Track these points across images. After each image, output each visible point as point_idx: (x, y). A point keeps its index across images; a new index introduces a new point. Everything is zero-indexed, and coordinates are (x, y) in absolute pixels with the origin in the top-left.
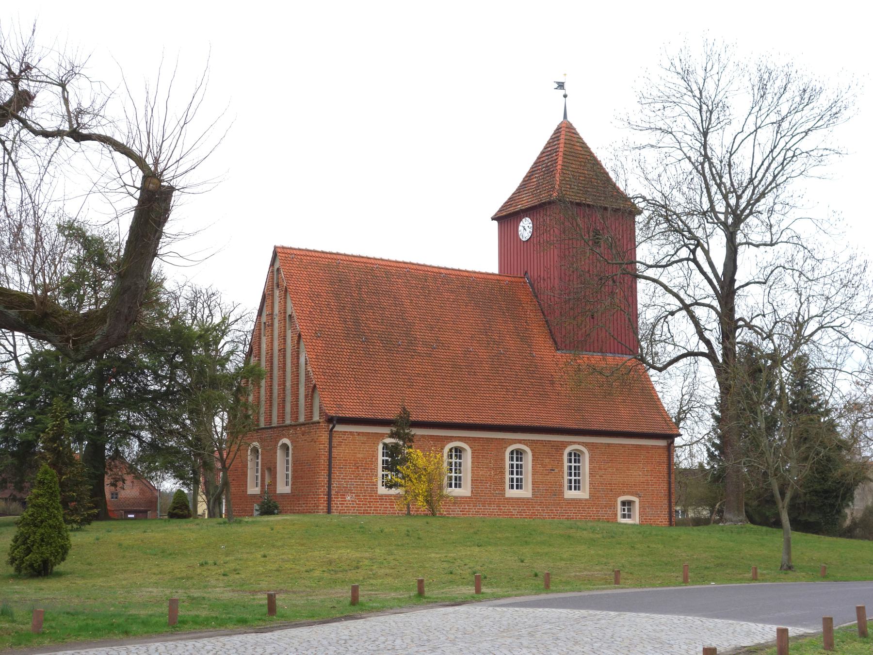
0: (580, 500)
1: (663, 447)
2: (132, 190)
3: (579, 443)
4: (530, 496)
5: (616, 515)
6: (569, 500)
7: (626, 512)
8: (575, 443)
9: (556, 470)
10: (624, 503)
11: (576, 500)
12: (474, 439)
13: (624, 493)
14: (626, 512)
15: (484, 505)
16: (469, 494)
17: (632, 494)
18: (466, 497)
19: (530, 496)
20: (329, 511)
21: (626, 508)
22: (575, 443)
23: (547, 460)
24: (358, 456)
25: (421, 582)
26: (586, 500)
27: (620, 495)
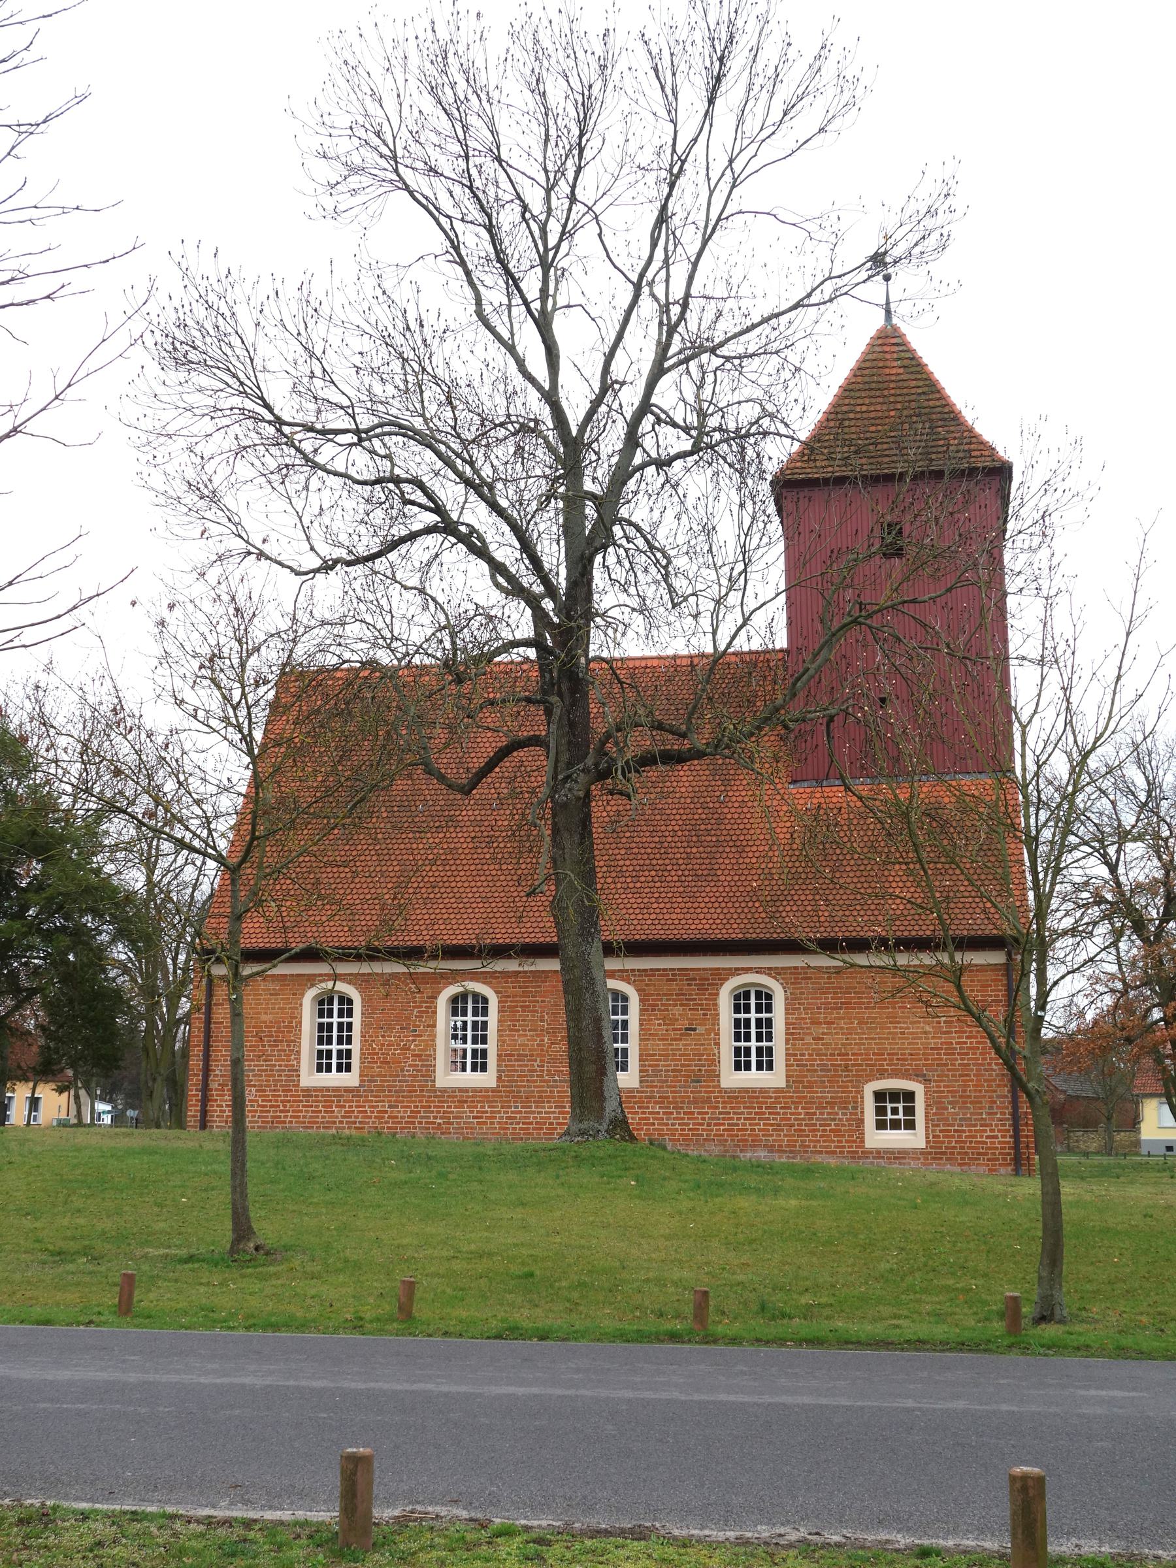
0: (763, 1091)
1: (994, 967)
2: (447, 544)
3: (758, 971)
4: (783, 1085)
5: (861, 1121)
6: (733, 1090)
7: (901, 1116)
8: (752, 972)
9: (701, 1030)
10: (879, 1096)
11: (754, 1090)
12: (505, 974)
13: (882, 1074)
14: (901, 1116)
15: (526, 1103)
16: (493, 1084)
17: (906, 1075)
18: (487, 1090)
19: (783, 1085)
20: (204, 1125)
21: (900, 1106)
22: (738, 971)
23: (678, 1010)
24: (264, 1017)
25: (410, 1287)
26: (778, 1090)
27: (870, 1078)
